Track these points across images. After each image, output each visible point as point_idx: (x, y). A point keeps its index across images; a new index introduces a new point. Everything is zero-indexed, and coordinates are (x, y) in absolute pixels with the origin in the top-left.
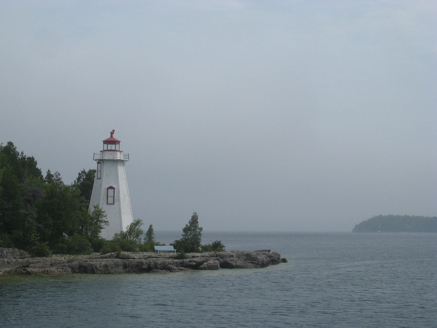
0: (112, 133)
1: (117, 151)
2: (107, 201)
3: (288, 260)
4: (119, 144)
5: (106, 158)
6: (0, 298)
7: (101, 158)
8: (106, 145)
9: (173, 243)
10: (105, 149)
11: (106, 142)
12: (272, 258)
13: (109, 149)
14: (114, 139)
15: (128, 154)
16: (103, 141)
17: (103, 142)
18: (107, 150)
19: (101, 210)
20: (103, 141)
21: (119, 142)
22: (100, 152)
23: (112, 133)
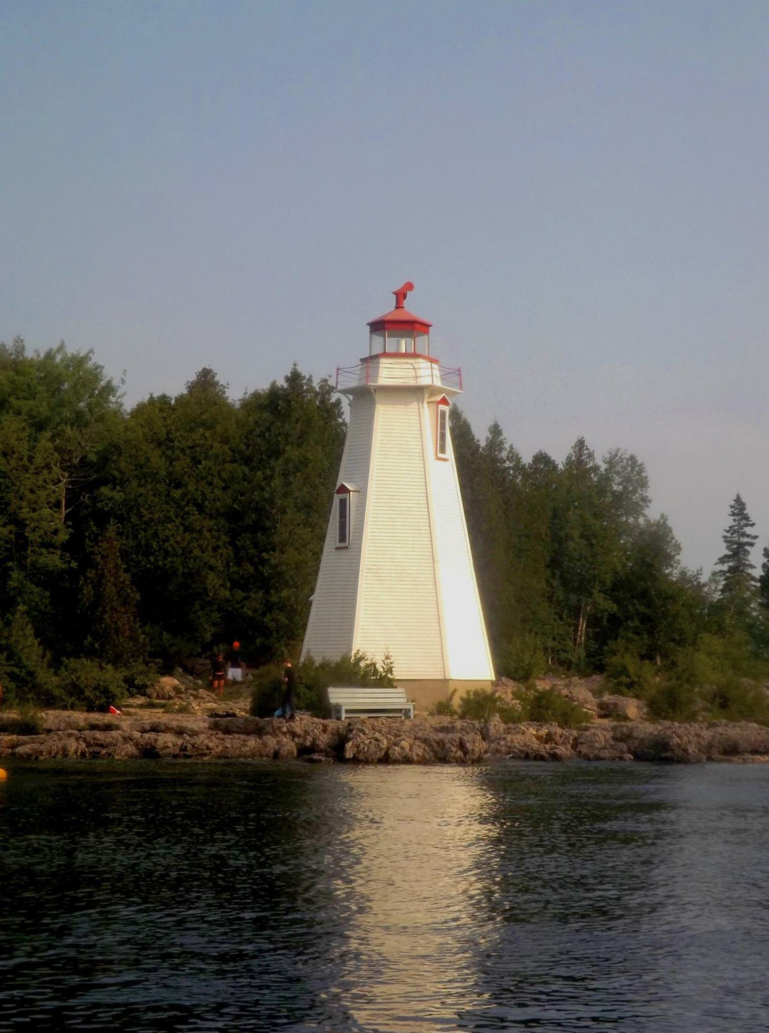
1: (377, 356)
8: (378, 340)
10: (378, 349)
11: (379, 327)
16: (368, 324)
18: (385, 355)
20: (368, 324)
21: (428, 326)
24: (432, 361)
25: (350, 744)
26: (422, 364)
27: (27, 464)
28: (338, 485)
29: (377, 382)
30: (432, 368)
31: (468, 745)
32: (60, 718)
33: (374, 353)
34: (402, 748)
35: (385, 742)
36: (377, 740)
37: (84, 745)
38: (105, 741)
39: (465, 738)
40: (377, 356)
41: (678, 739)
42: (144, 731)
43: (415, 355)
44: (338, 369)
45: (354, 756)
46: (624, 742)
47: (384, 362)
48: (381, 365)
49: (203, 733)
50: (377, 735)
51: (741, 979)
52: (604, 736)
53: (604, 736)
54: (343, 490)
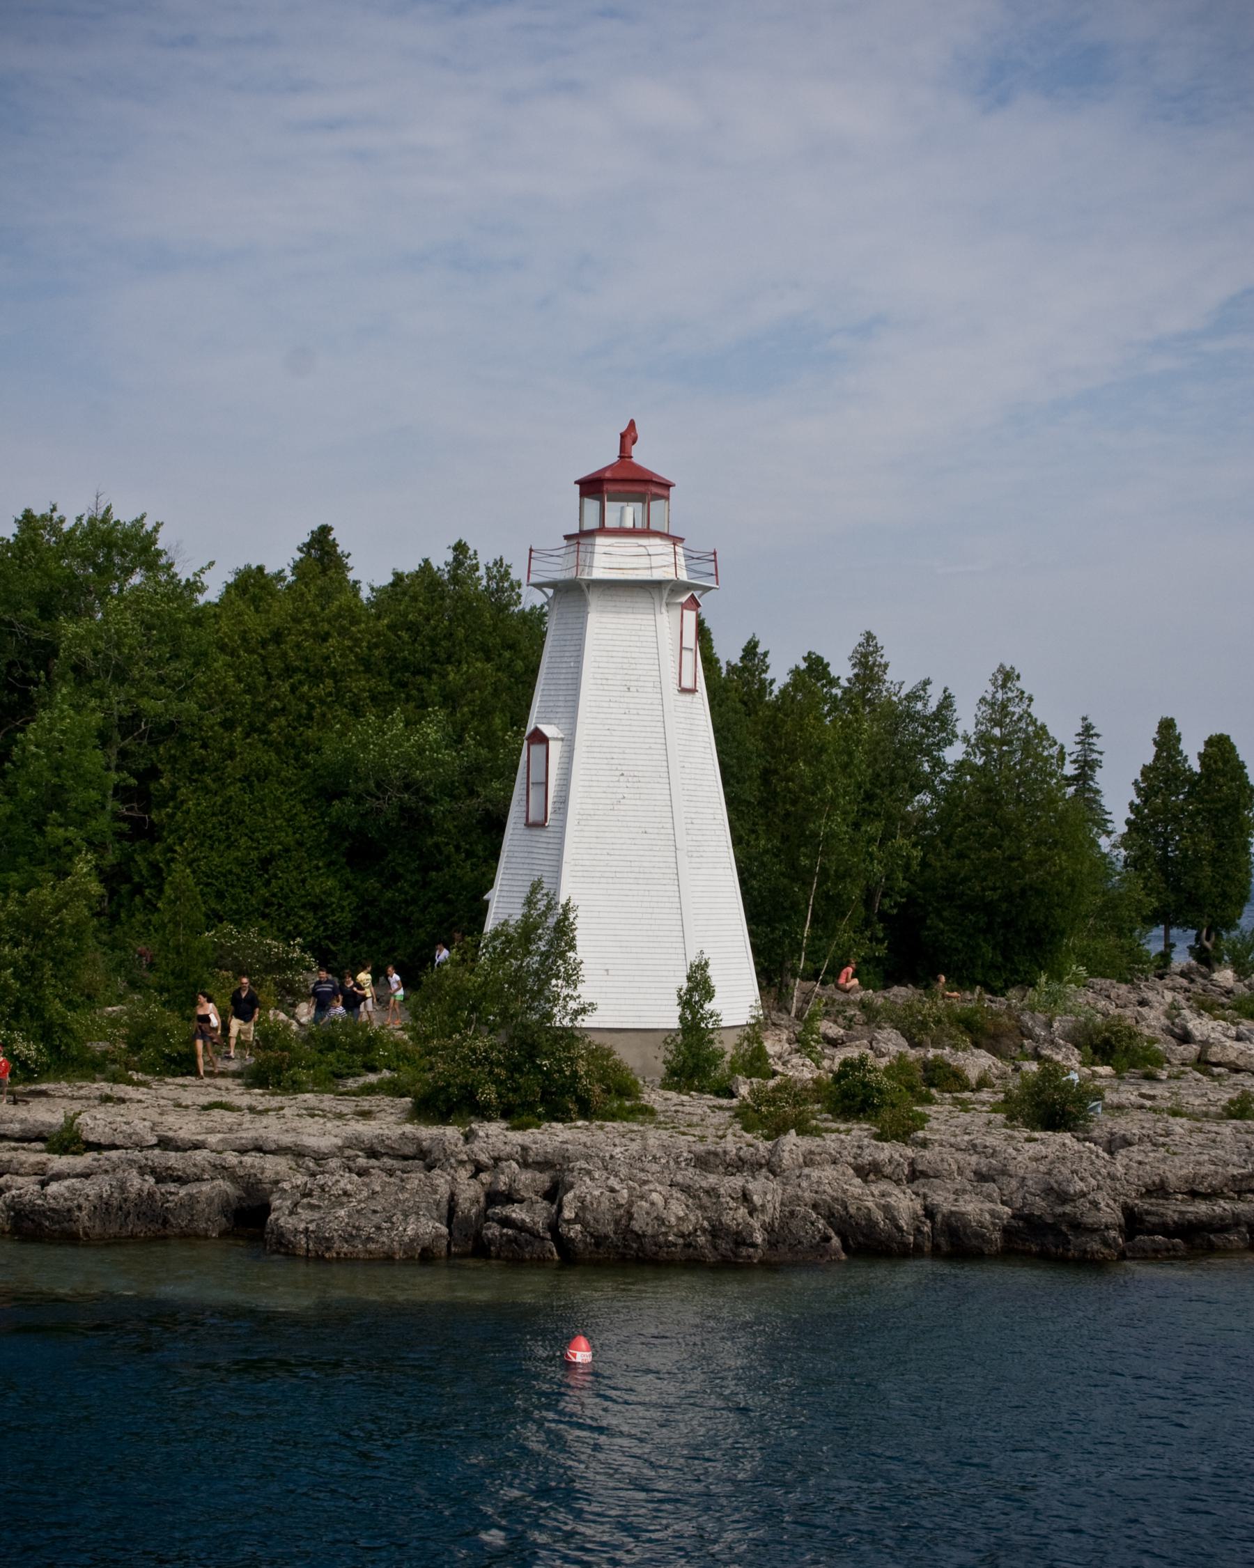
0: (628, 437)
1: (591, 534)
2: (524, 809)
3: (693, 958)
4: (667, 498)
5: (598, 574)
6: (1, 655)
7: (568, 575)
8: (592, 506)
9: (12, 540)
10: (591, 523)
11: (592, 487)
12: (1068, 1209)
13: (611, 522)
14: (639, 469)
15: (715, 554)
16: (576, 482)
17: (578, 487)
18: (603, 531)
19: (567, 904)
20: (576, 482)
21: (667, 486)
22: (565, 543)
23: (628, 437)
24: (676, 540)
25: (570, 1195)
26: (656, 545)
27: (116, 736)
28: (530, 728)
29: (590, 573)
30: (675, 553)
31: (755, 1197)
32: (114, 1126)
33: (587, 527)
34: (653, 1204)
35: (625, 1193)
36: (612, 1190)
37: (152, 1180)
38: (184, 1172)
39: (750, 1186)
40: (591, 534)
41: (1082, 1184)
42: (243, 1151)
43: (647, 533)
44: (531, 550)
45: (577, 1214)
46: (994, 1181)
47: (602, 543)
48: (597, 549)
49: (333, 1155)
50: (613, 1182)
51: (1146, 1552)
52: (957, 1162)
53: (957, 1162)
54: (540, 738)
